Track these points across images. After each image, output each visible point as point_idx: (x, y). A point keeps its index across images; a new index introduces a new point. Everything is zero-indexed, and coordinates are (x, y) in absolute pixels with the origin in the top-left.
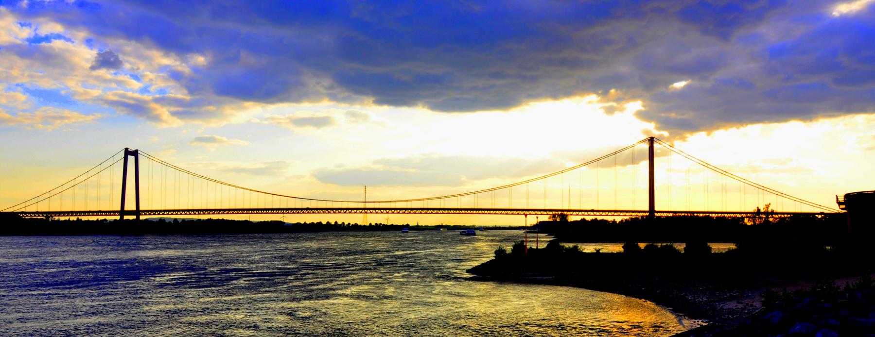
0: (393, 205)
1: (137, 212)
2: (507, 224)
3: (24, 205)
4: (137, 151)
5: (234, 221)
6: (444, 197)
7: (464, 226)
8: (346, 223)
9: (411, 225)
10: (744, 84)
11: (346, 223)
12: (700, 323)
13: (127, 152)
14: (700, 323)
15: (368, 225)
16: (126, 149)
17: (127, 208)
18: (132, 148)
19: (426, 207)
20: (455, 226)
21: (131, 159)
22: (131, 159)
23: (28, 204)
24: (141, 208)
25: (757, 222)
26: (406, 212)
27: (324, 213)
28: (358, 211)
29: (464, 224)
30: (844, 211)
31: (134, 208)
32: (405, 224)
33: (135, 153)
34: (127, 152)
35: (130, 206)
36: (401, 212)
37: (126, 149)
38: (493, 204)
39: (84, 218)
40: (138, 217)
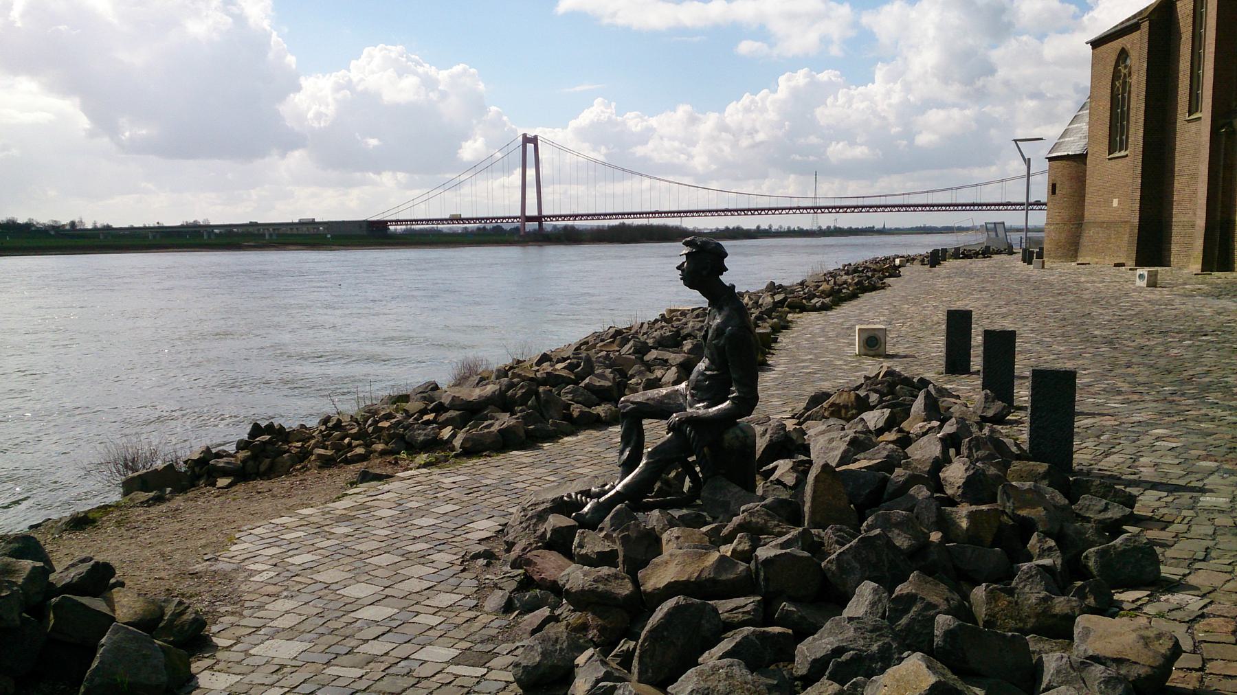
0: (883, 201)
1: (539, 218)
2: (939, 225)
3: (394, 211)
4: (536, 138)
5: (108, 228)
6: (957, 188)
7: (917, 227)
8: (792, 228)
9: (877, 227)
10: (881, 667)
11: (792, 228)
12: (757, 457)
13: (526, 140)
14: (757, 457)
15: (755, 228)
16: (525, 136)
17: (528, 214)
18: (531, 134)
19: (930, 202)
20: (896, 229)
21: (530, 146)
22: (530, 146)
23: (401, 208)
24: (544, 213)
25: (322, 125)
26: (871, 210)
27: (725, 215)
28: (791, 212)
29: (849, 226)
30: (715, 372)
31: (535, 213)
32: (854, 227)
33: (534, 140)
34: (526, 140)
35: (532, 211)
36: (856, 210)
37: (525, 136)
38: (979, 197)
39: (628, 222)
40: (540, 225)
